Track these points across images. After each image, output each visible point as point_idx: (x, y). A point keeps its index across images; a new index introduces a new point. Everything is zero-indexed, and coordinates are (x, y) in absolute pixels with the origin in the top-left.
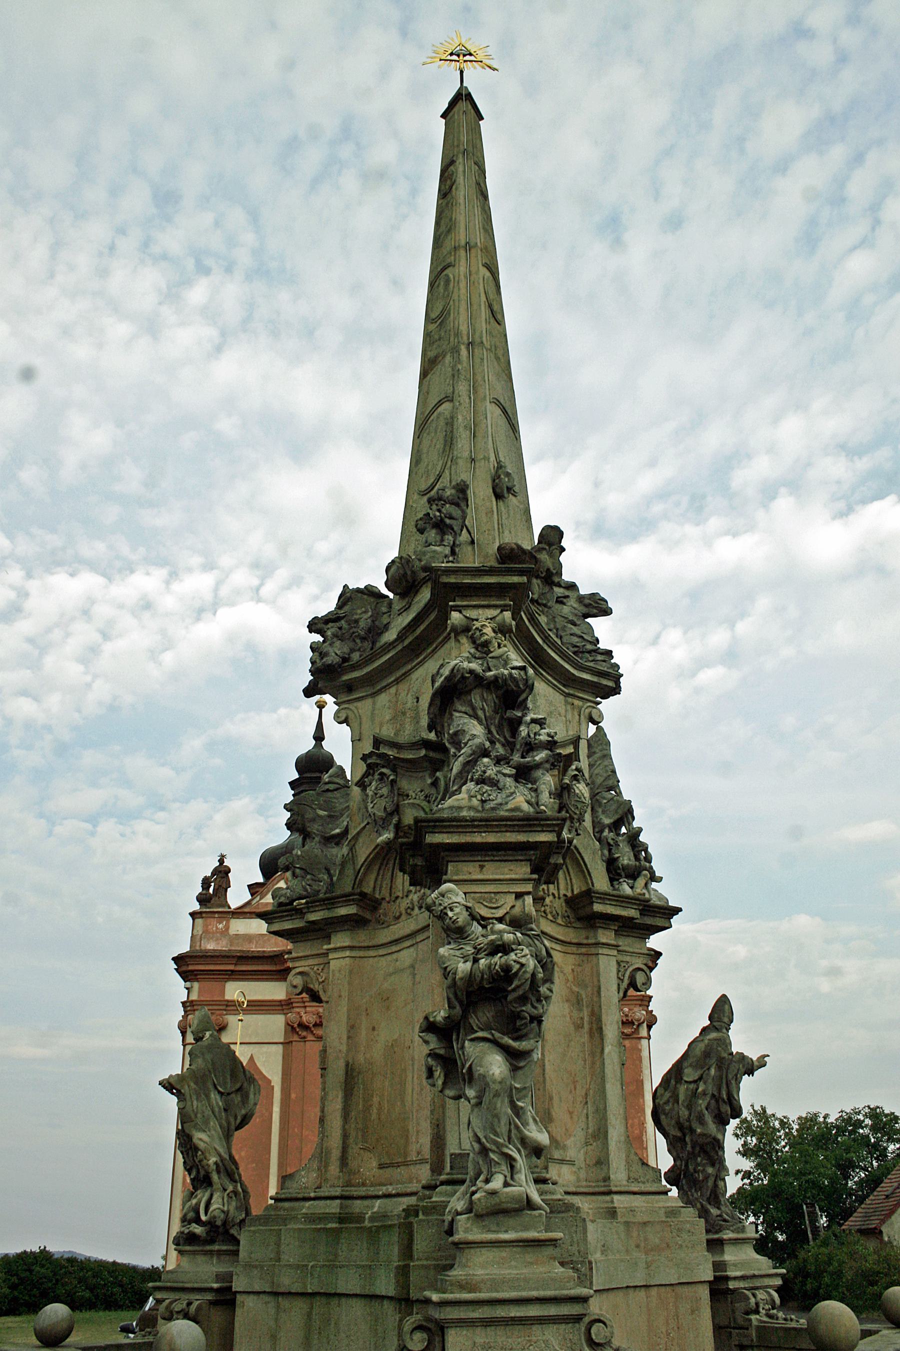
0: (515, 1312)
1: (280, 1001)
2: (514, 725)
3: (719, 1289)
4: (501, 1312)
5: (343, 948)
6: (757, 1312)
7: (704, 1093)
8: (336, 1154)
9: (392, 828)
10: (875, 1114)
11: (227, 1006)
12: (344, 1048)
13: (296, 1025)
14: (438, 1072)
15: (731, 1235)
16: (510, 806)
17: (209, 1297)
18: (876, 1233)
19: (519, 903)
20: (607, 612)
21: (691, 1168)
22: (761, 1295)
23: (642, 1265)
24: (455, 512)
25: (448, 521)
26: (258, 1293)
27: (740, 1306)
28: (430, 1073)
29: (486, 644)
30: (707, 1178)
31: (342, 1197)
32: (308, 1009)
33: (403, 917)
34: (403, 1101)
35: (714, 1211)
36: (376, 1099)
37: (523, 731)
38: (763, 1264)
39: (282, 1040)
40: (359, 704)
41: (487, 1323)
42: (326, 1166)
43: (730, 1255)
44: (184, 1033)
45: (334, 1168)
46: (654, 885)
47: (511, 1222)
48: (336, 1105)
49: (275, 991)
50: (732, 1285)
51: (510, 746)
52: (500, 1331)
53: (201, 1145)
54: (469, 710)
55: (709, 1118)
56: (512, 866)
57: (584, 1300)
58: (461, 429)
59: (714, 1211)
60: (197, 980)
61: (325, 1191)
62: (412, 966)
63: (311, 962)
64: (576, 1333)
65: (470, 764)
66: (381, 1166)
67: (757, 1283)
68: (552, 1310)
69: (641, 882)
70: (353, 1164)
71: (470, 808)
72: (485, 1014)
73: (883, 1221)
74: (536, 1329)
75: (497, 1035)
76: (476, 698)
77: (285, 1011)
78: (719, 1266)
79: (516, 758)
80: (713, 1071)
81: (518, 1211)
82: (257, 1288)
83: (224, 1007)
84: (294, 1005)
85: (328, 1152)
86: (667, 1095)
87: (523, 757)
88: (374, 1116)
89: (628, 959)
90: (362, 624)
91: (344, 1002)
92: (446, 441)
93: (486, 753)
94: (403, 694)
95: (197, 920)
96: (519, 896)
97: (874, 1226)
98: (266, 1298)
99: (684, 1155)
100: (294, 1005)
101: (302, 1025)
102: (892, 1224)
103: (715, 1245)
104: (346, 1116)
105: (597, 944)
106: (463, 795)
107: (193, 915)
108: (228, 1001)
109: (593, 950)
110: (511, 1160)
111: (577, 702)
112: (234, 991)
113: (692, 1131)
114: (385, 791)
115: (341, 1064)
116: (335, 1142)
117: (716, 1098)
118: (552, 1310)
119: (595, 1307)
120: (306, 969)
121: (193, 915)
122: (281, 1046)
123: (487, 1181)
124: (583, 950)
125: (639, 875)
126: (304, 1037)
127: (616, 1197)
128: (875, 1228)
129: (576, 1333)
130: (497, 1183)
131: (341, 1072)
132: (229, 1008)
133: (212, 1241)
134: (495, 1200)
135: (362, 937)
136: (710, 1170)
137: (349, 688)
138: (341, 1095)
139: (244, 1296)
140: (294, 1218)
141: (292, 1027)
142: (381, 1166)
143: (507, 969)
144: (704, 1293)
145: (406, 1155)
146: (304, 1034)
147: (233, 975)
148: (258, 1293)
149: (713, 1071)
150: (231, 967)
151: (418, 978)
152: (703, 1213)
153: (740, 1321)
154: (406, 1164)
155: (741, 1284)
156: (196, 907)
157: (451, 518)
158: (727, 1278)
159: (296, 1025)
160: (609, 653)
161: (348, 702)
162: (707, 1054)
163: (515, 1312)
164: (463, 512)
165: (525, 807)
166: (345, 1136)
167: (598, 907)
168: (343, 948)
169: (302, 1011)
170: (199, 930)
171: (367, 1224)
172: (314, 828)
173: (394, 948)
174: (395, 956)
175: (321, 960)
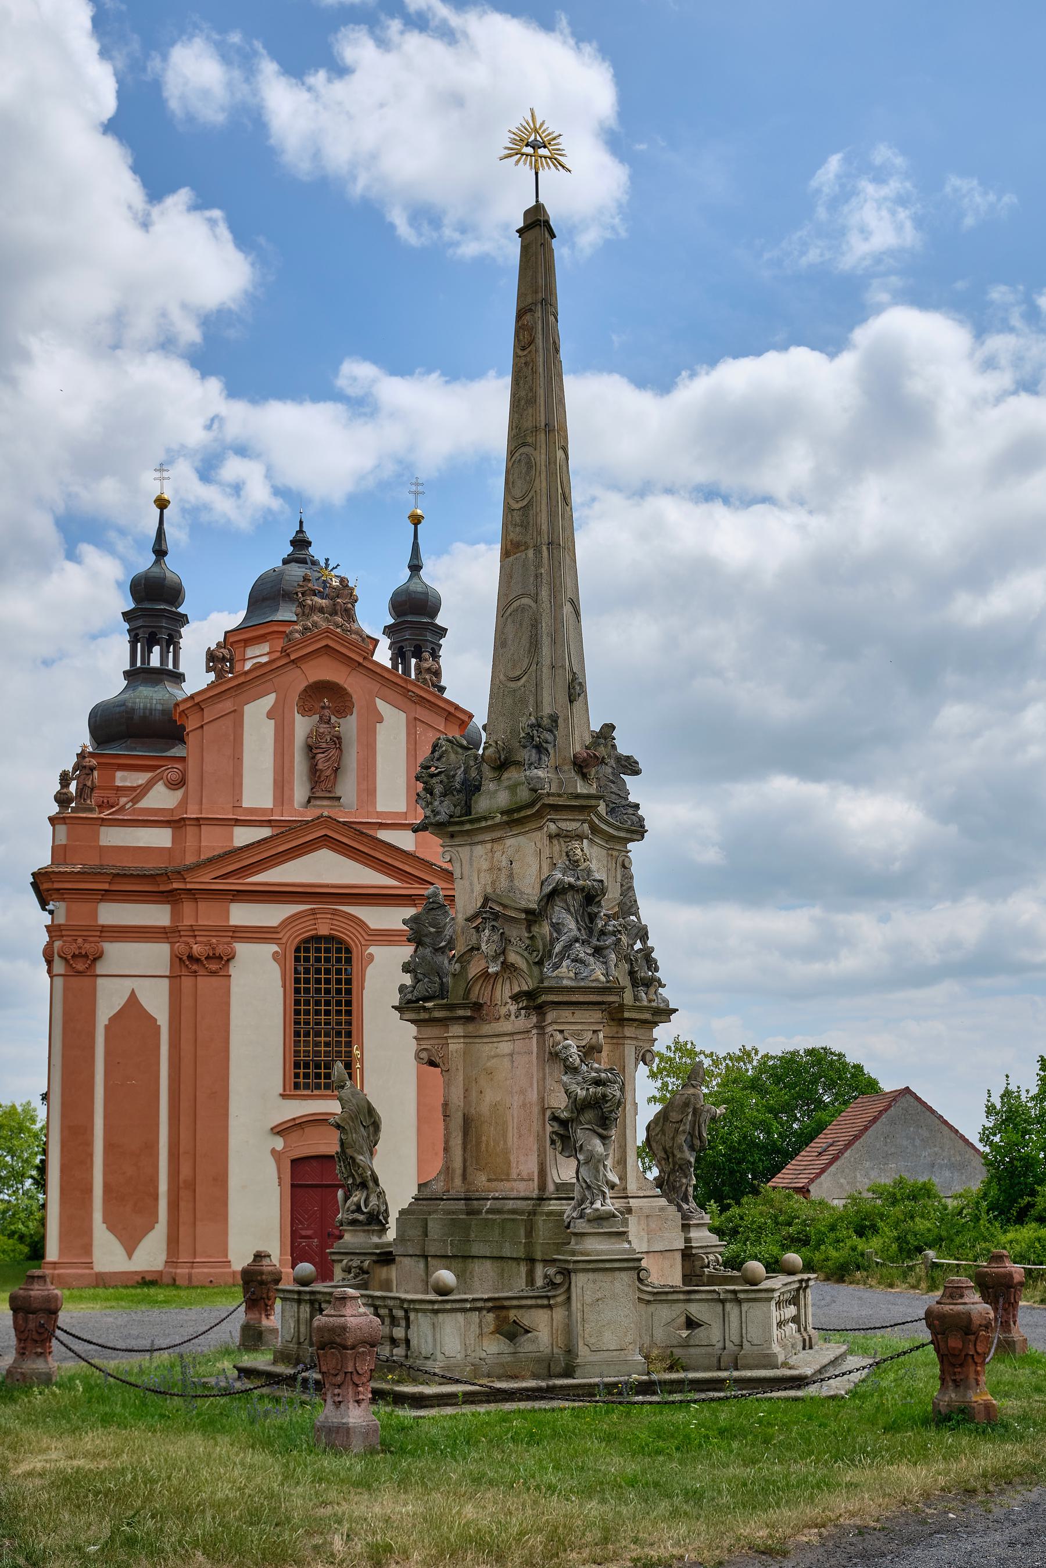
0: (608, 1265)
1: (164, 928)
2: (593, 917)
3: (687, 1254)
4: (601, 1265)
5: (459, 1037)
6: (708, 1267)
7: (684, 1132)
8: (459, 1172)
9: (499, 962)
10: (825, 1049)
11: (101, 931)
12: (462, 1104)
13: (185, 958)
14: (558, 1143)
15: (695, 1222)
16: (592, 978)
17: (374, 1258)
18: (804, 1191)
19: (595, 1036)
20: (637, 772)
21: (671, 1178)
22: (711, 1257)
23: (646, 1240)
24: (549, 736)
25: (544, 745)
26: (411, 1256)
27: (698, 1263)
28: (553, 1142)
29: (577, 861)
30: (681, 1186)
31: (465, 1199)
32: (198, 939)
33: (502, 1020)
34: (505, 1142)
35: (685, 1206)
36: (484, 1138)
37: (600, 924)
38: (714, 1240)
39: (168, 974)
40: (460, 849)
41: (594, 1270)
42: (452, 1179)
43: (694, 1234)
44: (49, 962)
45: (458, 1181)
46: (661, 990)
47: (605, 1223)
48: (457, 1141)
49: (158, 915)
50: (694, 1251)
51: (590, 932)
52: (601, 1274)
53: (362, 1164)
54: (564, 905)
55: (685, 1148)
56: (591, 1013)
57: (640, 1260)
58: (544, 637)
59: (685, 1206)
60: (63, 900)
61: (453, 1193)
62: (511, 1055)
63: (432, 1042)
64: (634, 1274)
65: (568, 947)
66: (489, 1180)
67: (709, 1250)
68: (626, 1265)
69: (652, 990)
70: (470, 1178)
71: (570, 978)
72: (589, 1115)
73: (812, 1181)
74: (617, 1274)
75: (596, 1127)
76: (569, 897)
77: (171, 940)
78: (688, 1240)
79: (595, 942)
80: (690, 1117)
81: (607, 1218)
82: (411, 1253)
83: (98, 934)
84: (182, 933)
85: (454, 1171)
86: (658, 1129)
87: (598, 940)
88: (483, 1148)
89: (641, 1044)
90: (458, 779)
91: (461, 1073)
92: (531, 643)
93: (577, 940)
94: (498, 854)
95: (57, 827)
96: (594, 1032)
97: (801, 1185)
98: (417, 1259)
99: (667, 1170)
100: (182, 933)
101: (190, 957)
102: (821, 1184)
103: (686, 1227)
104: (465, 1149)
105: (624, 1037)
106: (564, 970)
107: (52, 820)
108: (103, 926)
109: (621, 1041)
110: (604, 1193)
111: (615, 853)
112: (111, 914)
113: (674, 1156)
114: (495, 938)
115: (460, 1114)
116: (457, 1164)
117: (691, 1135)
118: (626, 1265)
119: (644, 1264)
120: (429, 1047)
121: (52, 820)
122: (167, 980)
123: (592, 1203)
124: (615, 1041)
125: (651, 984)
126: (195, 972)
127: (631, 1200)
128: (803, 1187)
129: (634, 1274)
130: (598, 1205)
131: (460, 1121)
132: (104, 934)
133: (369, 1224)
134: (598, 1213)
135: (471, 1028)
136: (684, 1181)
137: (452, 836)
138: (460, 1134)
139: (402, 1258)
140: (435, 1212)
141: (180, 959)
142: (489, 1180)
143: (604, 1096)
144: (678, 1256)
145: (508, 1175)
146: (195, 967)
147: (108, 896)
148: (411, 1256)
149: (690, 1117)
150: (106, 887)
151: (515, 1064)
152: (680, 1209)
153: (698, 1272)
154: (508, 1180)
155: (700, 1251)
156: (54, 809)
157: (547, 742)
158: (692, 1247)
159: (185, 958)
160: (637, 806)
161: (451, 846)
162: (686, 1104)
163: (608, 1265)
164: (555, 736)
165: (602, 978)
166: (465, 1161)
167: (626, 1015)
168: (459, 1037)
169: (191, 940)
170: (62, 840)
171: (484, 1216)
172: (427, 940)
173: (495, 1040)
174: (495, 1045)
175: (444, 1041)
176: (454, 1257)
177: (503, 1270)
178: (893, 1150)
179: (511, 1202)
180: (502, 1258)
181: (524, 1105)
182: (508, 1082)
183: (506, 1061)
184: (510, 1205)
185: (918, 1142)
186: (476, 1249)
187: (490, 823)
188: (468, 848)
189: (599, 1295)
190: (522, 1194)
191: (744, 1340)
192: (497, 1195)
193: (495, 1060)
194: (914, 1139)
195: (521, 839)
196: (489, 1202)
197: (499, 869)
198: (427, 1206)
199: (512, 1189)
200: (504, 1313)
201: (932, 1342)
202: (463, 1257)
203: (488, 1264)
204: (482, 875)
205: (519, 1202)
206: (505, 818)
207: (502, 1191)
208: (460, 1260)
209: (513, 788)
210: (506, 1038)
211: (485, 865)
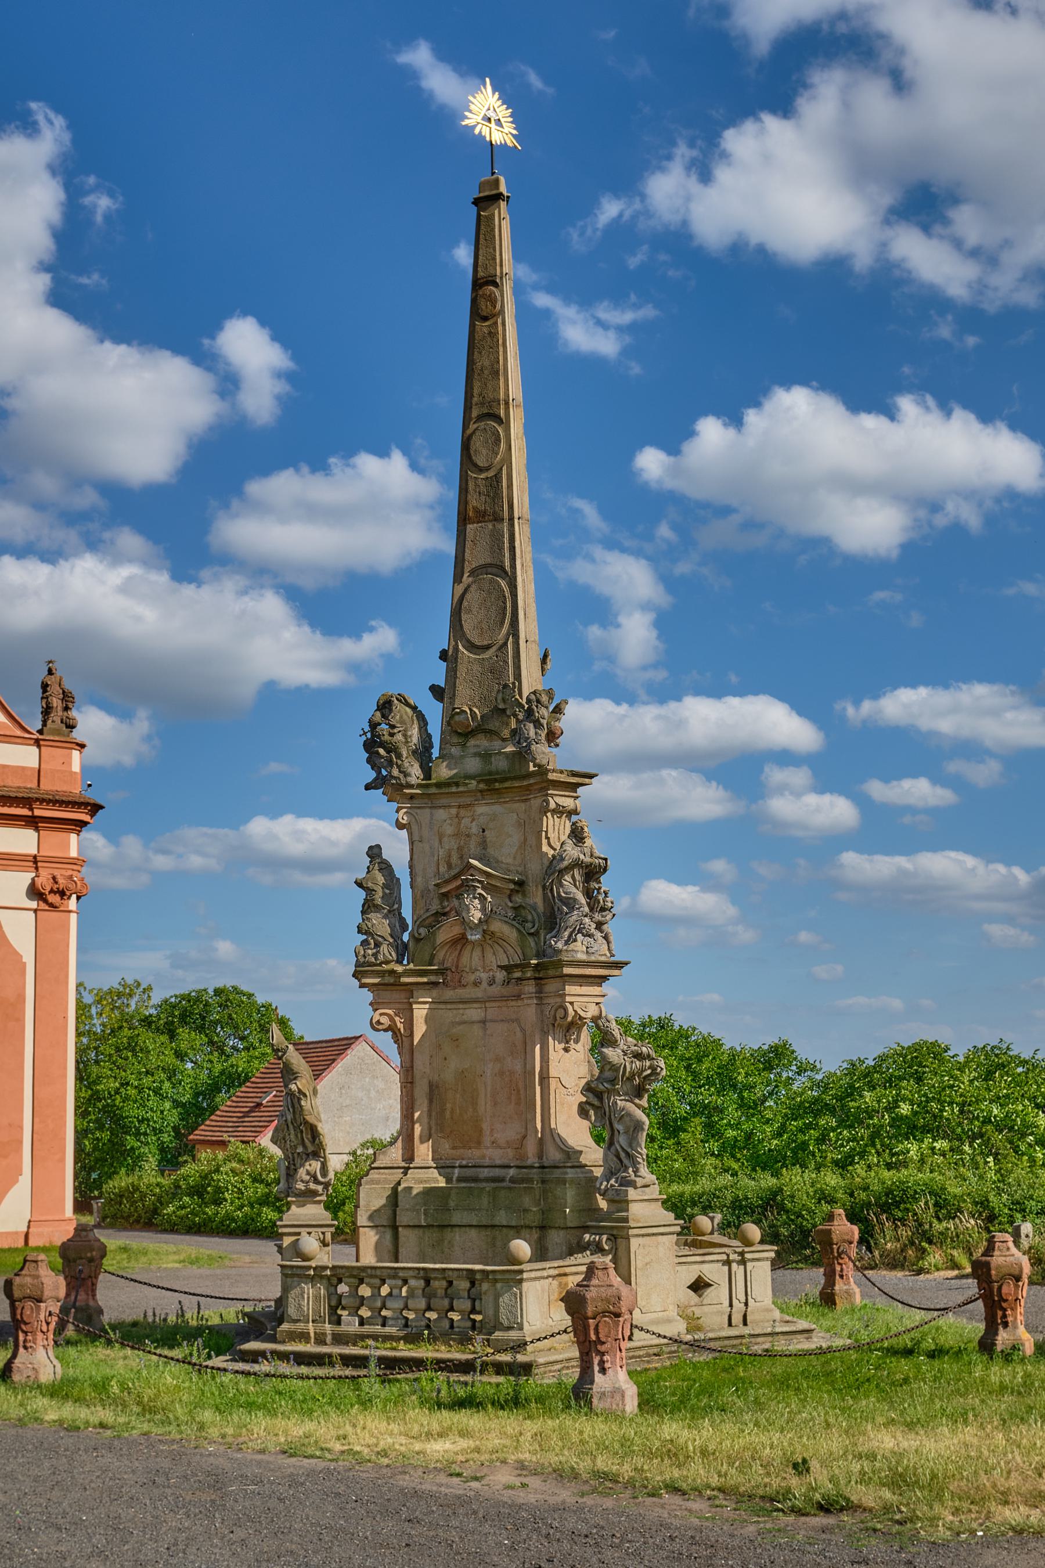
36: (449, 1106)
40: (418, 811)
62: (483, 1022)
88: (448, 1114)
94: (466, 821)
115: (425, 1081)
131: (426, 1088)
138: (426, 1102)
142: (454, 1148)
151: (488, 1032)
173: (461, 1006)
174: (461, 1011)
176: (429, 1226)
177: (494, 1238)
178: (348, 1102)
179: (486, 1170)
180: (493, 1226)
181: (501, 1073)
182: (479, 1050)
183: (477, 1029)
184: (485, 1173)
185: (373, 1094)
186: (457, 1218)
187: (461, 789)
188: (428, 810)
189: (647, 1260)
190: (498, 1162)
191: (749, 1298)
192: (464, 1163)
193: (461, 1027)
194: (369, 1091)
195: (497, 808)
196: (456, 1171)
197: (468, 836)
198: (389, 1174)
199: (484, 1157)
200: (564, 1279)
201: (981, 1296)
202: (439, 1226)
203: (473, 1233)
204: (445, 839)
205: (497, 1170)
206: (482, 786)
207: (470, 1159)
208: (436, 1229)
209: (486, 756)
210: (475, 1005)
211: (449, 830)
